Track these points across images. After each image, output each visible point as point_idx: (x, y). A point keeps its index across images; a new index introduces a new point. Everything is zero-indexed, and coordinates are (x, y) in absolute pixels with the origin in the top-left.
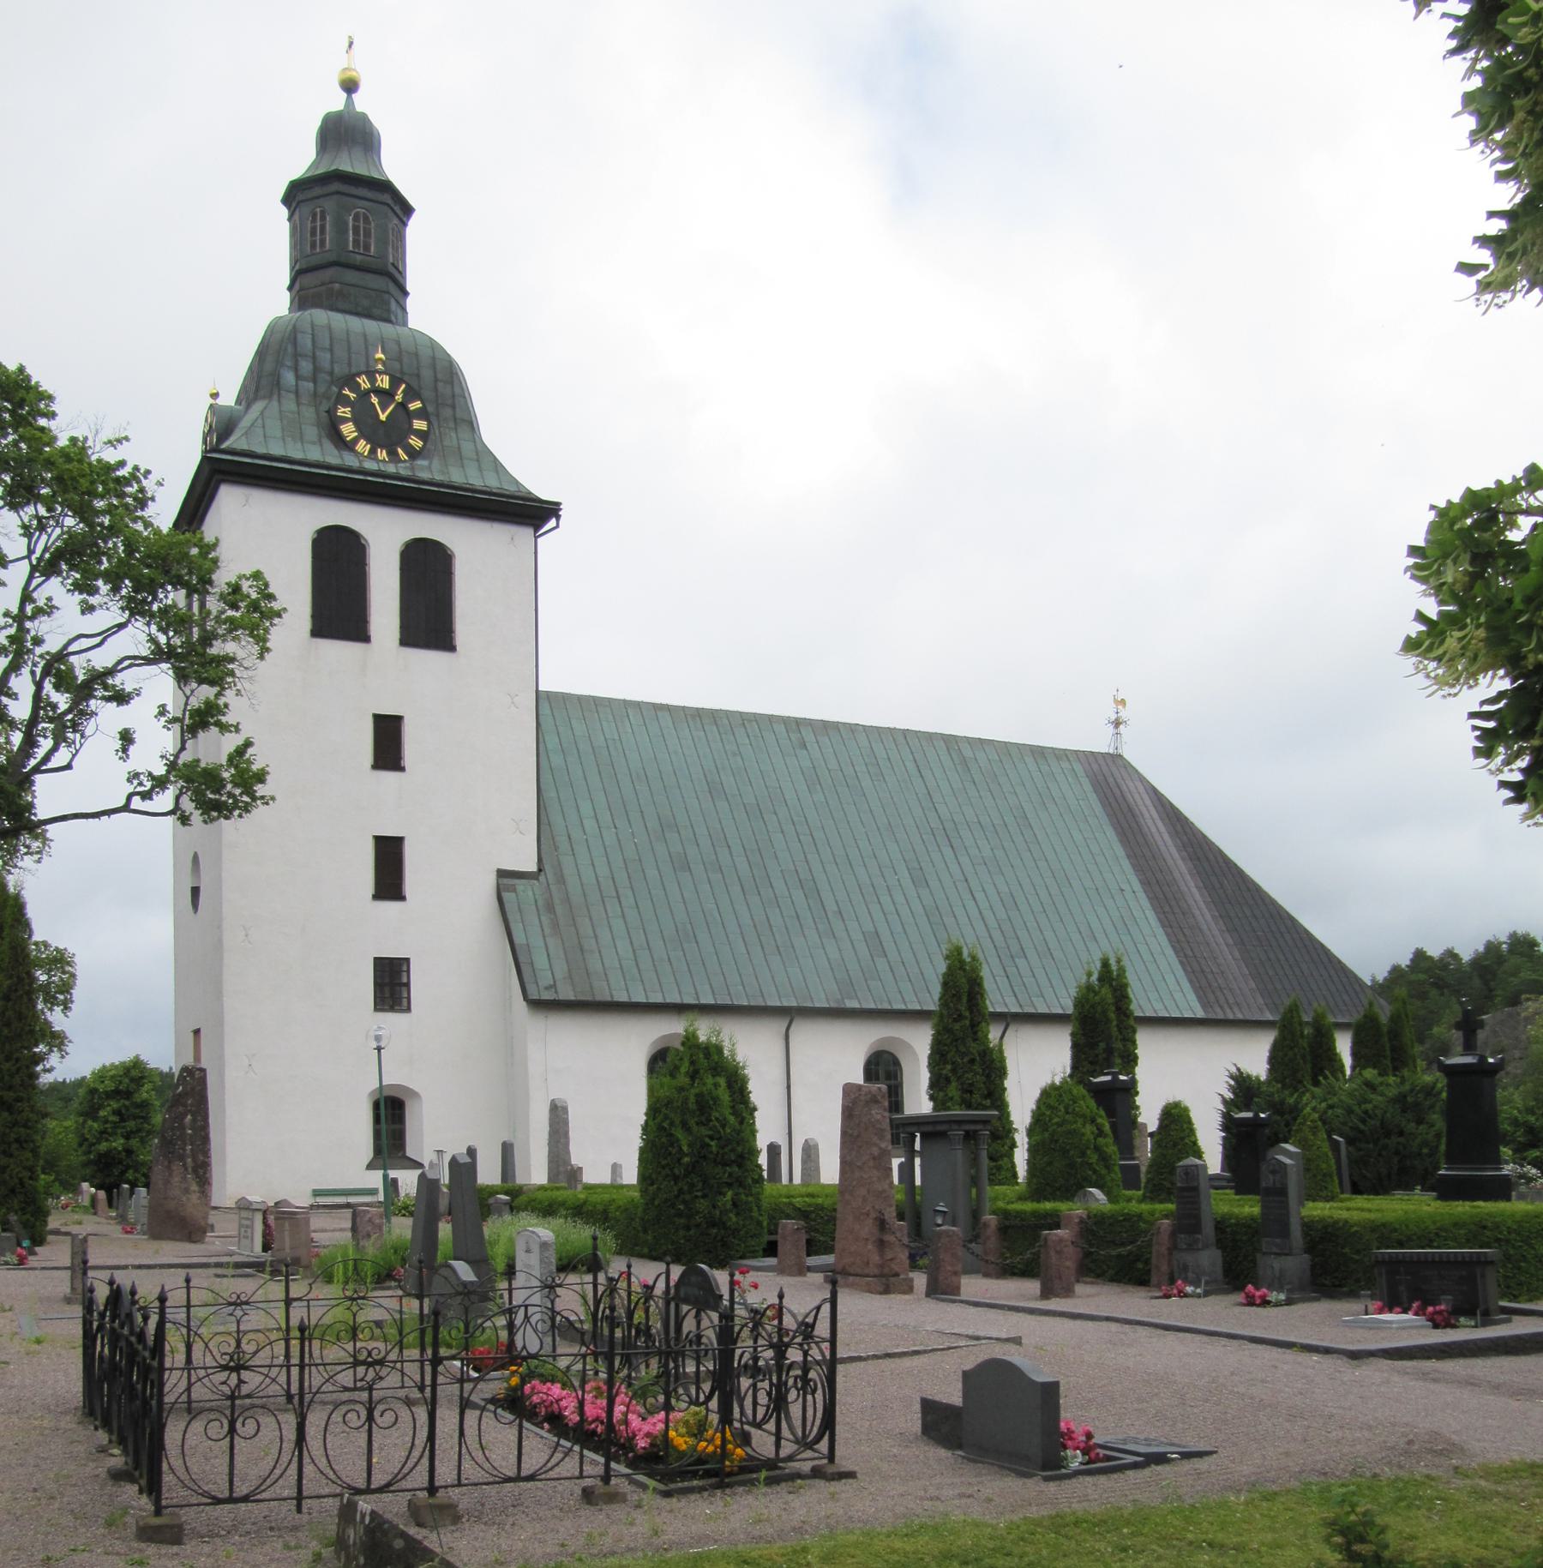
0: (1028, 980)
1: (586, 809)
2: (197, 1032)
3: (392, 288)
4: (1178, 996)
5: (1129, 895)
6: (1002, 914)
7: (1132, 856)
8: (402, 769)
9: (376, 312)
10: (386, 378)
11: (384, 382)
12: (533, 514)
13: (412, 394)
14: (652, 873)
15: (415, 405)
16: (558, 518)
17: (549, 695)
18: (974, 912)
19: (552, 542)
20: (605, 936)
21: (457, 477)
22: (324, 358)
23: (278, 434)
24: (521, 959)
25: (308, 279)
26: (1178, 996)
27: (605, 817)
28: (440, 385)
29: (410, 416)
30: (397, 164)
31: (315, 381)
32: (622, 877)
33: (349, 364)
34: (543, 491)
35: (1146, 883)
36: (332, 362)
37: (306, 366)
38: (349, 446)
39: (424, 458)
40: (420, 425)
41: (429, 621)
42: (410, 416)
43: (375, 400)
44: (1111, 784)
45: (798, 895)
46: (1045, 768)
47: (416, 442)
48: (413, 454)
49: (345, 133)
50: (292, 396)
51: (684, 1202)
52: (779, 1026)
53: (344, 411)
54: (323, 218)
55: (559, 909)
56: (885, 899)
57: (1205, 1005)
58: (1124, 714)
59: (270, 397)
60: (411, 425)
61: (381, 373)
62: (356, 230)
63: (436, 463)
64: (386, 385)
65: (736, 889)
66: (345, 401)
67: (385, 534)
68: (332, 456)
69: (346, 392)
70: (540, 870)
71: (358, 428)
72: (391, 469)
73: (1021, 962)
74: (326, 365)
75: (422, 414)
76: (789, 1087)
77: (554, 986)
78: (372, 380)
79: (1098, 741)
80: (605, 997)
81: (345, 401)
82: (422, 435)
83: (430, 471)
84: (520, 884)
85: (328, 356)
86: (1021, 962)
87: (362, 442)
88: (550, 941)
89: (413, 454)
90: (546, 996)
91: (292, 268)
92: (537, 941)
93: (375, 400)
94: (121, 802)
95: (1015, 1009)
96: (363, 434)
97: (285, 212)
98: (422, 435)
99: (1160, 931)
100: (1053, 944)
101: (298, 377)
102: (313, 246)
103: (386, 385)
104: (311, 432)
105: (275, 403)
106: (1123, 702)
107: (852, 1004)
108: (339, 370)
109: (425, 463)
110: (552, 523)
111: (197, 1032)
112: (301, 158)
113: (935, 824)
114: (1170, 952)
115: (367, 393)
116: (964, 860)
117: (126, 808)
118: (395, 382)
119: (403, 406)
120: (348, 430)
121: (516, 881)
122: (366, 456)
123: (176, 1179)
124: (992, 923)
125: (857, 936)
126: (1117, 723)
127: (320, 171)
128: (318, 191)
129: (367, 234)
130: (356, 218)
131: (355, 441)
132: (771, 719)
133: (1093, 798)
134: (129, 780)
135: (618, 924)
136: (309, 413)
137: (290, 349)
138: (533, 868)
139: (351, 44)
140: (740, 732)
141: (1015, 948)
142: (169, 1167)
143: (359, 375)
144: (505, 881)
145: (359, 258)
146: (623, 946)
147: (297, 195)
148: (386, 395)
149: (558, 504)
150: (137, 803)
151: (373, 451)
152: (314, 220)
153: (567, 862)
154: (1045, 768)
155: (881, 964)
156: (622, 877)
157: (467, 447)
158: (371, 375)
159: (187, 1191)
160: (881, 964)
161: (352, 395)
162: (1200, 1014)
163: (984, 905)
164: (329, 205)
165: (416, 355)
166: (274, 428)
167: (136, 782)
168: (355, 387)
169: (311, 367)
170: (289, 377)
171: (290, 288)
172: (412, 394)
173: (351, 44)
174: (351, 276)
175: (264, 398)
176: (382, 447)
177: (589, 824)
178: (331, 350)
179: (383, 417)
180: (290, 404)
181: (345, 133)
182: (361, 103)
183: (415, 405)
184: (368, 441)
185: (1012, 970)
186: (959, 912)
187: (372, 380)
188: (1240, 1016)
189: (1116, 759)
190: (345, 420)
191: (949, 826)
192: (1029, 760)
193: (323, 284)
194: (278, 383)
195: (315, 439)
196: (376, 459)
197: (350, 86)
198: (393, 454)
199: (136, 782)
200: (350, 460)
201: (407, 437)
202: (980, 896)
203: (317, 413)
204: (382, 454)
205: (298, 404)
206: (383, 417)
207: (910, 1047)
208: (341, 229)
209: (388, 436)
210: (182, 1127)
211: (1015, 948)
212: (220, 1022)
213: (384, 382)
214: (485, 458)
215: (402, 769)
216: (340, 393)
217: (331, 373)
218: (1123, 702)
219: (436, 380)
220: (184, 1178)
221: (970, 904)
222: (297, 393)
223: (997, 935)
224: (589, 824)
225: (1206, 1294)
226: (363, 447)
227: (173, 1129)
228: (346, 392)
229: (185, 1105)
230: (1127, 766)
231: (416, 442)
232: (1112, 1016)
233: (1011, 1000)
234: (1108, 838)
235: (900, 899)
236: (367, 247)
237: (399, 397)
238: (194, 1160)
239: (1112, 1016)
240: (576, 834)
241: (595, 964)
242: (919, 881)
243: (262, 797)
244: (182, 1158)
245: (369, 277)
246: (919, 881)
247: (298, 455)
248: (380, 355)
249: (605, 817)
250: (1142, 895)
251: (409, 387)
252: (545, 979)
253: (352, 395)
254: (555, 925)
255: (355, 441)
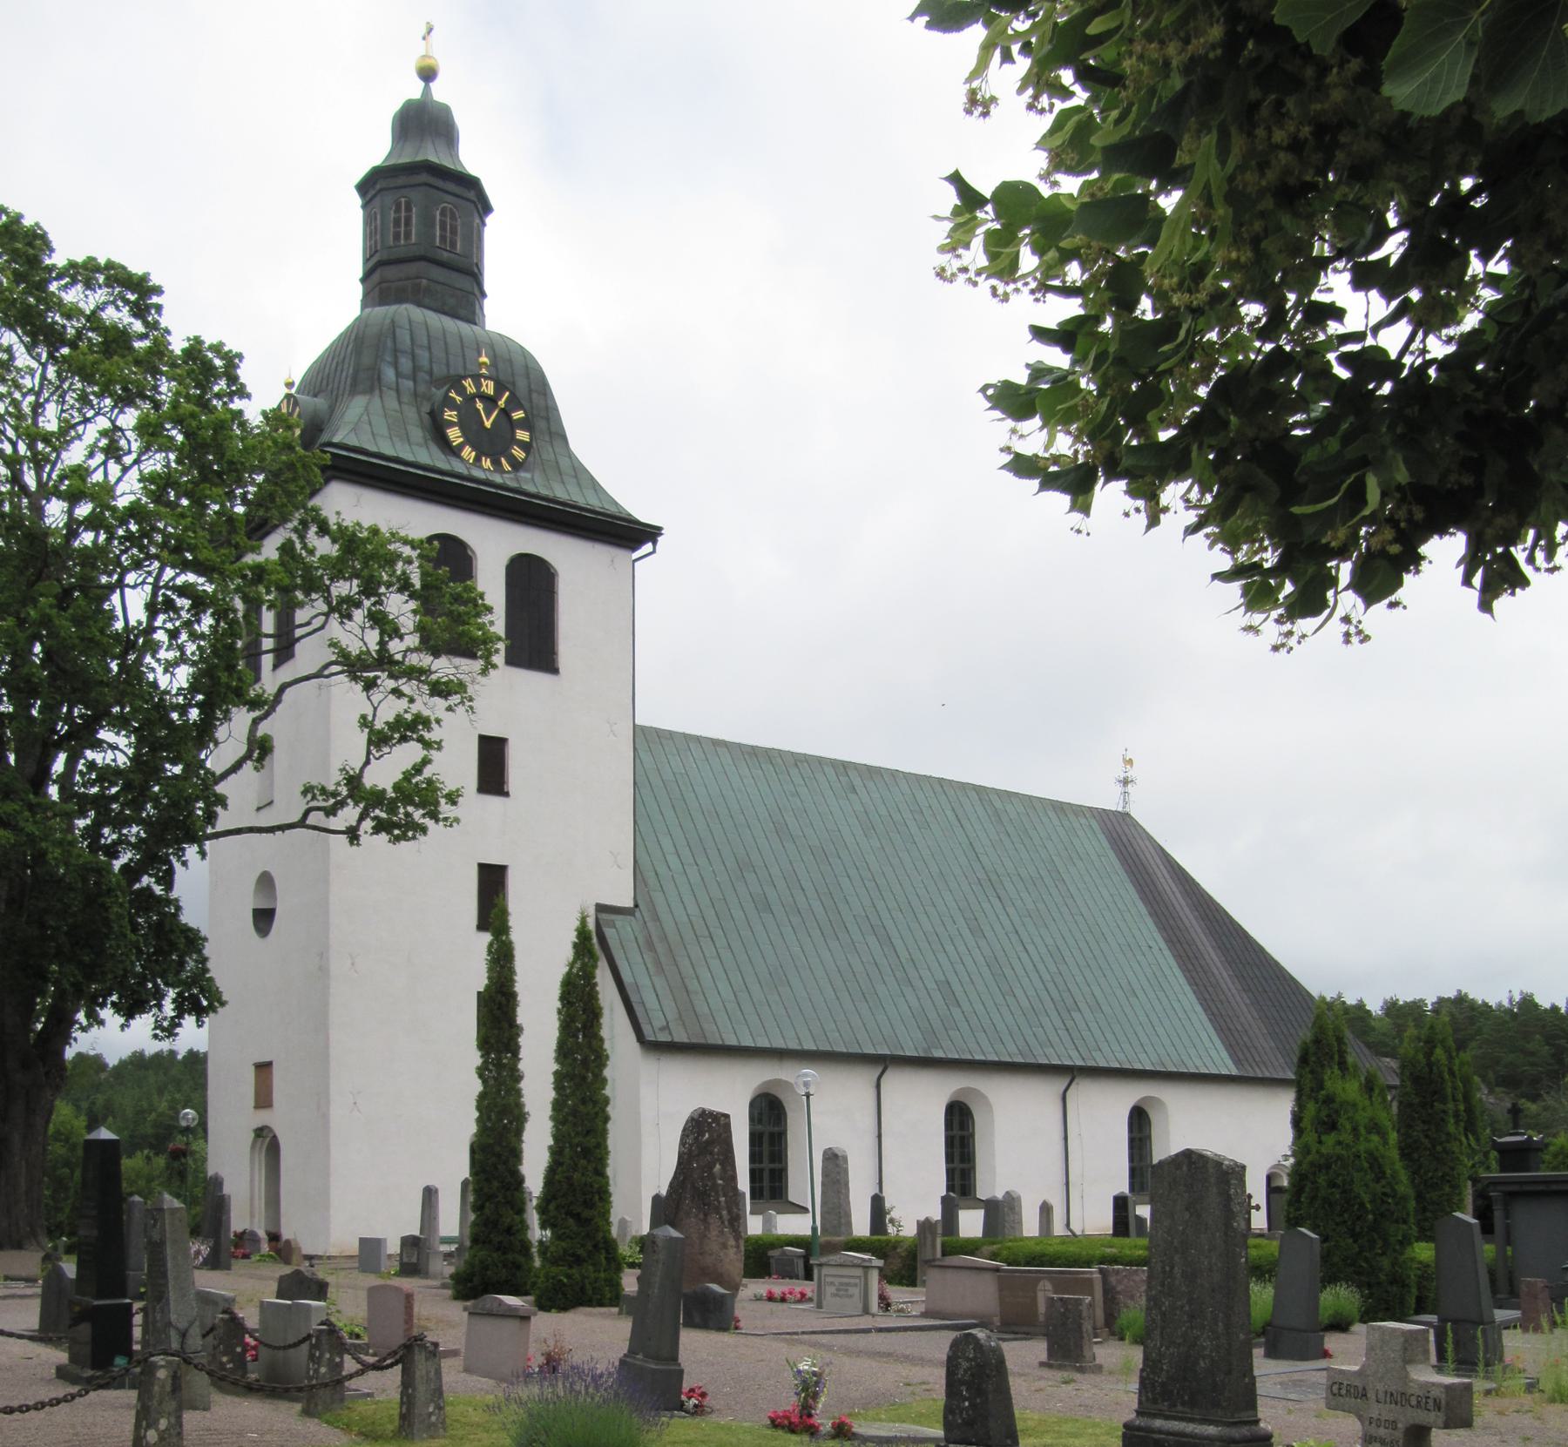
0: (1086, 1034)
1: (666, 843)
2: (264, 1068)
3: (476, 291)
4: (1213, 1053)
5: (1155, 950)
6: (1053, 969)
7: (1154, 914)
8: (507, 794)
9: (462, 312)
10: (491, 384)
11: (489, 388)
12: (631, 535)
13: (514, 403)
14: (738, 914)
15: (518, 415)
16: (655, 543)
17: (643, 728)
18: (1030, 967)
19: (650, 566)
20: (705, 975)
21: (560, 493)
22: (423, 356)
23: (385, 431)
24: (634, 998)
25: (391, 272)
26: (1213, 1053)
27: (685, 852)
28: (534, 395)
29: (514, 425)
30: (474, 155)
31: (415, 381)
32: (710, 914)
33: (448, 365)
34: (644, 515)
35: (1170, 942)
36: (431, 362)
37: (405, 364)
38: (455, 452)
39: (527, 471)
40: (522, 435)
41: (534, 645)
42: (514, 425)
43: (480, 406)
44: (1122, 836)
45: (872, 940)
46: (1066, 823)
47: (519, 453)
48: (516, 465)
49: (423, 122)
50: (393, 393)
51: (1366, 1260)
52: (871, 1074)
53: (450, 415)
54: (408, 209)
55: (660, 948)
56: (950, 948)
57: (1237, 1062)
58: (1131, 774)
59: (370, 391)
60: (514, 434)
61: (486, 378)
62: (443, 228)
63: (538, 477)
64: (491, 391)
65: (816, 933)
66: (452, 405)
67: (493, 545)
68: (440, 461)
69: (453, 394)
70: (636, 906)
71: (464, 434)
72: (498, 479)
73: (1076, 1015)
74: (425, 363)
75: (526, 424)
76: (880, 1136)
77: (666, 1028)
78: (478, 385)
79: (1109, 800)
80: (714, 1039)
81: (452, 405)
82: (526, 447)
83: (533, 483)
84: (619, 920)
85: (427, 354)
86: (1076, 1015)
87: (467, 449)
88: (656, 980)
89: (516, 465)
90: (663, 1037)
91: (366, 261)
92: (644, 981)
93: (480, 406)
94: (296, 818)
95: (1079, 1063)
96: (469, 440)
97: (357, 201)
98: (526, 447)
99: (1187, 988)
100: (1102, 1000)
101: (398, 375)
102: (397, 236)
103: (491, 391)
104: (417, 433)
105: (377, 400)
106: (1130, 762)
107: (938, 1054)
108: (439, 370)
109: (528, 475)
110: (648, 547)
111: (264, 1068)
112: (377, 148)
113: (981, 875)
114: (1199, 1008)
115: (472, 398)
116: (1011, 910)
117: (302, 823)
118: (500, 387)
119: (505, 413)
120: (454, 435)
121: (613, 917)
122: (470, 463)
123: (714, 1233)
124: (1047, 977)
125: (931, 985)
126: (1126, 782)
127: (392, 162)
128: (401, 181)
129: (454, 232)
130: (443, 213)
131: (461, 447)
132: (820, 761)
133: (1111, 854)
134: (304, 793)
135: (715, 963)
136: (411, 413)
137: (389, 343)
138: (629, 904)
139: (430, 30)
140: (793, 772)
141: (1069, 1001)
142: (705, 1221)
143: (465, 378)
144: (604, 916)
145: (446, 254)
146: (723, 986)
147: (373, 186)
148: (490, 401)
149: (660, 529)
150: (316, 818)
151: (478, 459)
152: (398, 210)
153: (658, 897)
154: (1066, 823)
155: (956, 1012)
156: (710, 914)
157: (564, 463)
158: (477, 379)
159: (724, 1246)
160: (956, 1012)
161: (459, 399)
162: (1234, 1072)
163: (1036, 958)
164: (416, 196)
165: (510, 361)
166: (381, 427)
167: (309, 796)
168: (461, 391)
169: (410, 364)
170: (389, 374)
171: (364, 280)
172: (514, 403)
173: (430, 30)
174: (437, 273)
175: (364, 392)
176: (487, 456)
177: (673, 861)
178: (429, 348)
179: (488, 424)
180: (392, 403)
181: (423, 122)
182: (440, 92)
183: (518, 415)
184: (474, 448)
185: (1070, 1023)
186: (1015, 963)
187: (478, 385)
188: (1267, 1075)
189: (1126, 816)
190: (452, 424)
191: (994, 877)
192: (1051, 814)
193: (408, 279)
194: (379, 379)
195: (421, 441)
196: (481, 467)
197: (428, 74)
198: (496, 463)
199: (309, 796)
200: (459, 468)
201: (509, 447)
202: (1030, 947)
203: (419, 412)
204: (487, 463)
205: (400, 403)
206: (488, 424)
207: (984, 1097)
208: (428, 222)
209: (493, 444)
210: (712, 1177)
211: (1069, 1001)
212: (321, 1058)
213: (489, 388)
214: (580, 473)
215: (507, 794)
216: (446, 396)
217: (431, 373)
218: (1130, 762)
219: (530, 391)
220: (722, 1232)
221: (1024, 955)
222: (398, 391)
223: (1051, 986)
224: (673, 861)
225: (1105, 1340)
226: (468, 453)
227: (702, 1178)
228: (453, 394)
229: (711, 1153)
230: (1136, 825)
231: (519, 453)
232: (1447, 1076)
233: (1074, 1054)
234: (1130, 894)
235: (962, 949)
236: (453, 244)
237: (502, 403)
238: (729, 1212)
239: (1447, 1076)
240: (662, 870)
241: (702, 1008)
242: (978, 931)
243: (446, 819)
244: (717, 1210)
245: (455, 275)
246: (978, 931)
247: (409, 457)
248: (484, 359)
249: (685, 852)
250: (1167, 953)
251: (513, 395)
252: (659, 1022)
253: (459, 399)
254: (658, 963)
255: (461, 447)
